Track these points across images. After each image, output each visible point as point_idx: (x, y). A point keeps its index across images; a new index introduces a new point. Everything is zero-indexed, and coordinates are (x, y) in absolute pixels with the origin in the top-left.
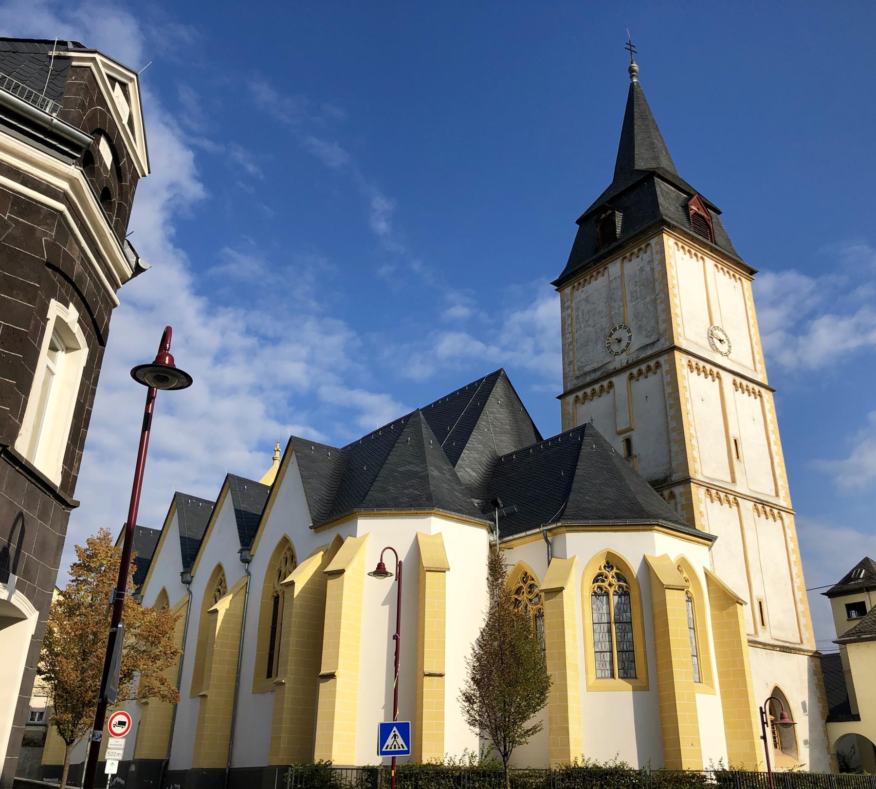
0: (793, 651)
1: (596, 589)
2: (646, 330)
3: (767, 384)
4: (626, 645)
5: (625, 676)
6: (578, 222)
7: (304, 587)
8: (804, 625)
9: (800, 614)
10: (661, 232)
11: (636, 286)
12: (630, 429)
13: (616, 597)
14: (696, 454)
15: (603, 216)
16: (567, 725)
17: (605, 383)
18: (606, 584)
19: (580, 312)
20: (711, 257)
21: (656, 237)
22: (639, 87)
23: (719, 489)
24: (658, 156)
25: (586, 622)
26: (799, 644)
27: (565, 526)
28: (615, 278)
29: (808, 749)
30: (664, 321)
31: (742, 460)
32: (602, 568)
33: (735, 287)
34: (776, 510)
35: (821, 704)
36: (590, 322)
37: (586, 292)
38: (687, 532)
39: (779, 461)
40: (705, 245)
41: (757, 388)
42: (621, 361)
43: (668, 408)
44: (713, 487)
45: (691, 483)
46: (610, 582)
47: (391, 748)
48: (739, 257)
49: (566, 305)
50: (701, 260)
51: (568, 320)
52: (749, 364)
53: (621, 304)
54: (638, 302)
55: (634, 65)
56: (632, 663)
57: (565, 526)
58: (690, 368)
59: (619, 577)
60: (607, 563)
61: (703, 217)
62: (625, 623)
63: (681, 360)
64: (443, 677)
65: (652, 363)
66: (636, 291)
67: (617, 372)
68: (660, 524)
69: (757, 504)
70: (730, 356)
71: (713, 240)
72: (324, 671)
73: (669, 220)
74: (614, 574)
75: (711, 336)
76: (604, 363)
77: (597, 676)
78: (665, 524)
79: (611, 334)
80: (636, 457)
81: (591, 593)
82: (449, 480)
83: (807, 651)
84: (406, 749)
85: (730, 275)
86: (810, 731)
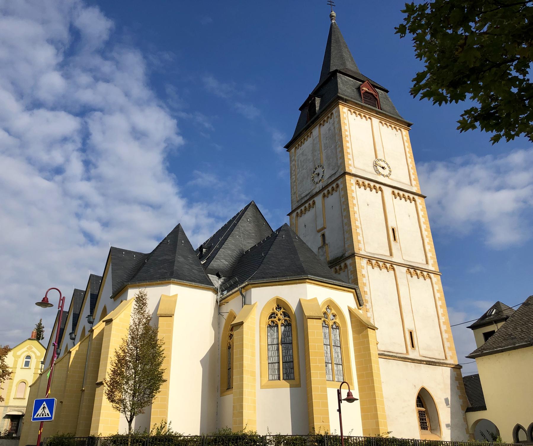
1: (270, 323)
3: (420, 193)
4: (289, 358)
5: (288, 378)
6: (300, 109)
7: (100, 332)
9: (445, 340)
10: (337, 105)
11: (327, 140)
12: (324, 228)
13: (283, 327)
14: (360, 238)
15: (310, 101)
17: (311, 202)
18: (276, 319)
20: (376, 117)
23: (378, 260)
24: (345, 62)
25: (262, 344)
26: (443, 360)
27: (251, 284)
28: (316, 137)
29: (450, 431)
30: (340, 158)
31: (398, 241)
32: (275, 309)
36: (304, 167)
37: (303, 149)
38: (333, 283)
40: (372, 110)
41: (411, 196)
42: (319, 187)
43: (343, 210)
44: (373, 258)
45: (356, 257)
47: (40, 416)
48: (399, 116)
49: (292, 159)
52: (408, 182)
53: (319, 153)
54: (328, 150)
55: (333, 12)
56: (292, 370)
57: (251, 284)
58: (359, 186)
59: (285, 314)
60: (278, 306)
61: (372, 94)
62: (288, 343)
63: (350, 180)
65: (334, 185)
66: (327, 143)
67: (317, 194)
70: (391, 177)
72: (99, 381)
73: (343, 96)
74: (282, 313)
75: (375, 165)
77: (269, 379)
78: (313, 278)
79: (314, 171)
82: (192, 264)
83: (450, 364)
84: (50, 416)
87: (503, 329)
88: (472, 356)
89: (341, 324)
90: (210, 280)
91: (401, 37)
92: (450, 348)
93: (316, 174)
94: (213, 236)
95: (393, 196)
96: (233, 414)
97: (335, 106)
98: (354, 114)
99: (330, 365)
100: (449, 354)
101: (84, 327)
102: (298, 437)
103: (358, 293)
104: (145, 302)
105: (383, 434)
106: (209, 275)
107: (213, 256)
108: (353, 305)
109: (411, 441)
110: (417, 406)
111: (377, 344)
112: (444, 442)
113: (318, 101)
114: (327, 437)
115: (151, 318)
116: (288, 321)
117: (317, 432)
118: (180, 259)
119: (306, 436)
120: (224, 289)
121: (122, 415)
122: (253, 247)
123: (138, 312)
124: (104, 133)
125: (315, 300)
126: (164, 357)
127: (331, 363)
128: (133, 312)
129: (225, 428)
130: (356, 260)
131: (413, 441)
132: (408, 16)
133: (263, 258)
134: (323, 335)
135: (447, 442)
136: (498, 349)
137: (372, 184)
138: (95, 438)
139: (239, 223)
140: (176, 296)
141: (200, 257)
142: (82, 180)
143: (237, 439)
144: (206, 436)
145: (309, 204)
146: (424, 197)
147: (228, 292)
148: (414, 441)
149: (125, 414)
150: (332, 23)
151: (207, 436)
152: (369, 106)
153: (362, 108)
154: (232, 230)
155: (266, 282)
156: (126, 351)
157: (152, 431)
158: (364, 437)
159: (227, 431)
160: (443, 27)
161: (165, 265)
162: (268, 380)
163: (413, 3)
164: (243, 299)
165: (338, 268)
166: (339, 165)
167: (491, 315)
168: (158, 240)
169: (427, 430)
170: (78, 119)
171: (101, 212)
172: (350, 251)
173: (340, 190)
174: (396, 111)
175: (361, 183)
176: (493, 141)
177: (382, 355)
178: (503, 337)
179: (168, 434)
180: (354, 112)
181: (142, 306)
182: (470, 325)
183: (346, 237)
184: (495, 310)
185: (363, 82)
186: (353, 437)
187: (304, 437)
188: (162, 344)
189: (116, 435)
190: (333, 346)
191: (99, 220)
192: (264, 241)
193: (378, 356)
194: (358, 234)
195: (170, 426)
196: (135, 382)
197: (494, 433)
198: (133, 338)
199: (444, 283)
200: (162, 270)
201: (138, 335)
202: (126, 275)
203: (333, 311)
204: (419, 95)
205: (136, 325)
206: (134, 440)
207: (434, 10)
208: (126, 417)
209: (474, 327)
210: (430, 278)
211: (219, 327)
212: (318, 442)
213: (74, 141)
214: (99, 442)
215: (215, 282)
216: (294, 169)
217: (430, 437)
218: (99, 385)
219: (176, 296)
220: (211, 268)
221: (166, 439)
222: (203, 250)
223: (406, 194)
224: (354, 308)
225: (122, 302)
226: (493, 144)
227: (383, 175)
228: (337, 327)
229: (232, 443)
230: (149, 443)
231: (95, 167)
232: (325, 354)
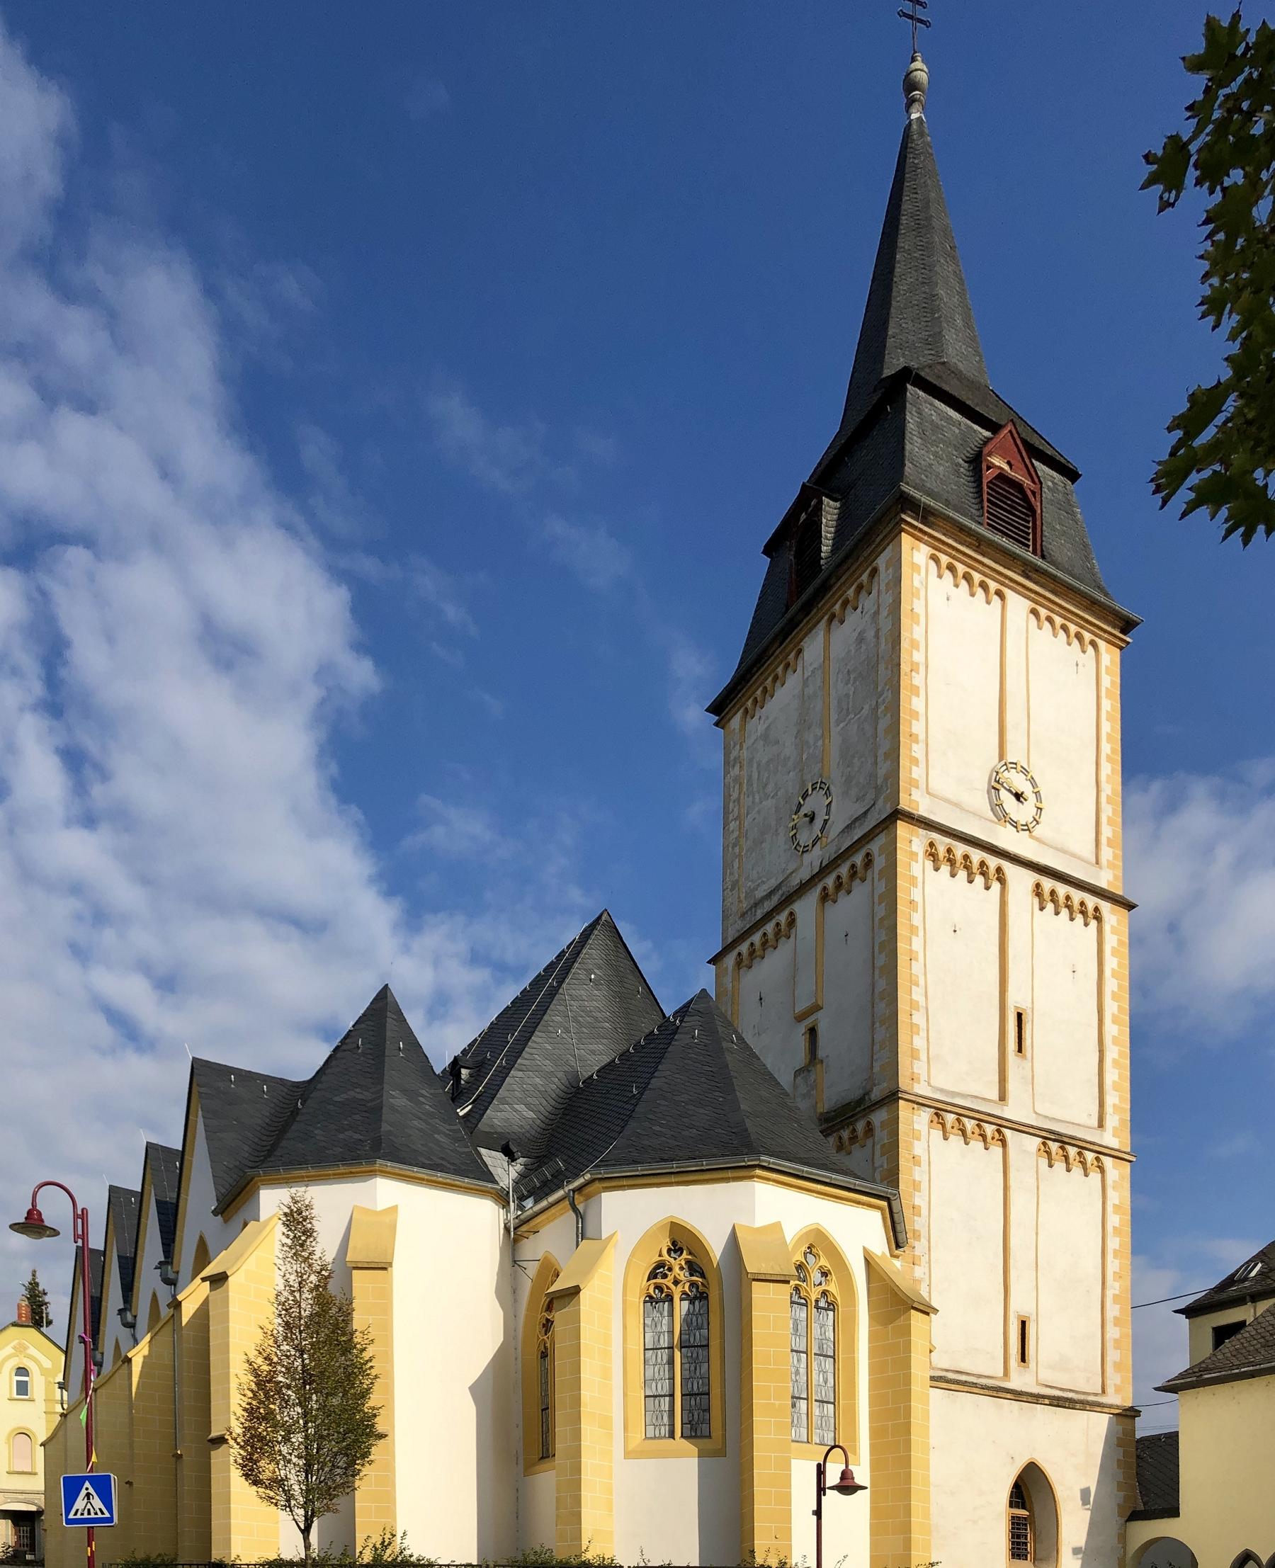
0: (1078, 1406)
1: (651, 1291)
3: (1119, 892)
5: (693, 1434)
6: (767, 551)
12: (816, 1008)
13: (686, 1304)
14: (919, 1042)
15: (803, 516)
16: (579, 1509)
17: (782, 918)
18: (668, 1282)
21: (888, 545)
22: (922, 134)
23: (962, 1113)
26: (1096, 1395)
27: (600, 1179)
30: (887, 756)
31: (1029, 1055)
33: (1077, 665)
34: (1008, 1130)
36: (770, 788)
38: (828, 1180)
41: (1091, 901)
44: (949, 1108)
46: (675, 1276)
47: (82, 1514)
48: (1100, 588)
50: (996, 599)
51: (734, 791)
52: (1087, 850)
53: (819, 733)
57: (600, 1179)
59: (693, 1268)
60: (674, 1243)
61: (1018, 486)
62: (697, 1346)
63: (910, 841)
64: (386, 1438)
65: (858, 859)
67: (804, 887)
68: (765, 1164)
69: (1050, 1143)
70: (1038, 831)
71: (1038, 547)
74: (683, 1263)
75: (995, 786)
76: (788, 872)
77: (647, 1436)
78: (773, 1163)
79: (800, 806)
83: (1110, 1406)
84: (107, 1515)
85: (955, 576)
90: (486, 1166)
91: (1165, 205)
92: (1118, 1366)
93: (806, 815)
95: (1036, 900)
99: (803, 1404)
100: (1113, 1379)
101: (154, 1295)
104: (309, 1226)
106: (483, 1151)
108: (878, 1243)
110: (1011, 1506)
111: (931, 1351)
113: (830, 511)
115: (331, 1272)
116: (701, 1288)
118: (395, 1099)
120: (525, 1193)
121: (284, 1516)
122: (606, 1066)
123: (294, 1254)
125: (776, 1227)
126: (376, 1377)
129: (538, 1549)
130: (901, 1113)
136: (1243, 1370)
137: (977, 855)
140: (394, 1209)
141: (453, 1094)
142: (68, 823)
147: (536, 1202)
149: (290, 1513)
154: (544, 1009)
156: (275, 1359)
157: (361, 1553)
159: (543, 1556)
164: (577, 1223)
165: (845, 1134)
167: (1246, 1279)
168: (327, 1039)
169: (1027, 1559)
171: (144, 940)
172: (885, 1085)
175: (942, 851)
177: (939, 1381)
178: (1263, 1337)
179: (400, 1558)
181: (303, 1238)
183: (878, 1037)
184: (1260, 1265)
185: (994, 427)
188: (366, 1342)
189: (275, 1560)
190: (815, 1354)
191: (144, 967)
193: (929, 1382)
194: (914, 1029)
195: (404, 1541)
198: (287, 1325)
200: (349, 1133)
203: (823, 1262)
204: (1184, 495)
205: (294, 1291)
209: (1191, 1312)
210: (1102, 1169)
211: (515, 1301)
216: (735, 795)
218: (217, 1443)
219: (394, 1209)
222: (460, 1073)
223: (1077, 896)
224: (879, 1254)
225: (245, 1225)
227: (1015, 824)
228: (829, 1304)
232: (793, 1375)
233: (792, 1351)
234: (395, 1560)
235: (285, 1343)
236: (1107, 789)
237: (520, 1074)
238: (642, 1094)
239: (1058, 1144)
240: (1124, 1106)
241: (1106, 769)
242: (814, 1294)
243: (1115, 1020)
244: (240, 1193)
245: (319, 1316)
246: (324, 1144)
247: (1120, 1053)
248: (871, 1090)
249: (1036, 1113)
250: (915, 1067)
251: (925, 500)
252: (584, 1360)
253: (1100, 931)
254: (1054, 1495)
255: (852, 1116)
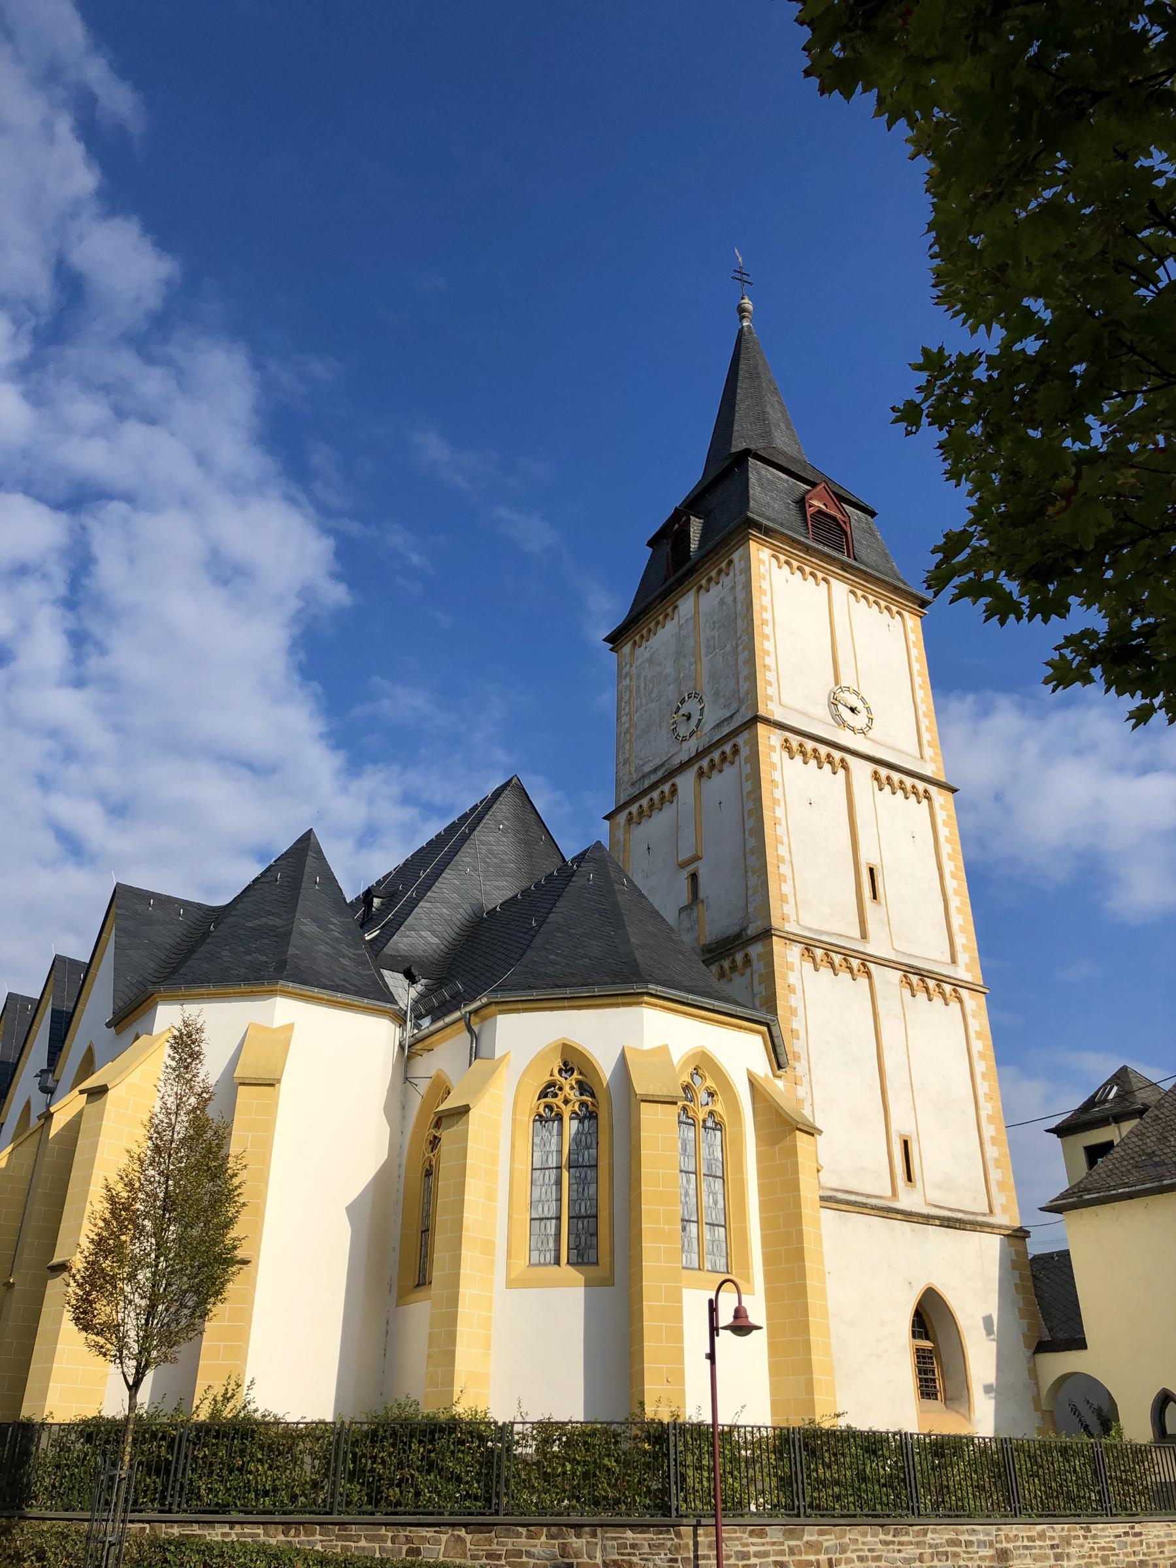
0: (968, 1227)
2: (724, 696)
3: (943, 779)
5: (580, 1260)
6: (650, 544)
8: (998, 1182)
9: (991, 1165)
10: (745, 540)
12: (696, 858)
13: (575, 1123)
14: (786, 889)
15: (677, 526)
17: (666, 788)
18: (558, 1101)
19: (642, 679)
23: (829, 948)
26: (984, 1215)
27: (497, 1003)
29: (993, 1402)
30: (746, 678)
32: (556, 1072)
35: (1025, 1321)
36: (654, 695)
38: (711, 1007)
39: (959, 905)
40: (831, 560)
41: (921, 786)
44: (818, 944)
48: (900, 580)
50: (823, 583)
52: (913, 748)
55: (746, 300)
57: (497, 1003)
59: (583, 1088)
60: (565, 1064)
61: (834, 518)
62: (586, 1166)
65: (727, 748)
67: (683, 767)
68: (654, 992)
69: (910, 976)
70: (871, 734)
73: (760, 520)
74: (574, 1083)
75: (834, 702)
78: (660, 991)
79: (679, 708)
80: (703, 901)
81: (532, 1118)
82: (337, 940)
83: (1000, 1227)
86: (999, 1368)
87: (1133, 1140)
88: (1055, 1208)
89: (728, 1116)
90: (387, 986)
91: (908, 433)
92: (1001, 1185)
93: (683, 715)
94: (404, 864)
95: (875, 783)
96: (429, 1356)
97: (737, 543)
98: (785, 567)
99: (693, 1228)
100: (999, 1199)
101: (28, 1103)
102: (599, 1426)
103: (775, 1034)
104: (197, 1048)
105: (824, 1418)
106: (385, 972)
107: (399, 919)
108: (761, 1065)
109: (894, 1437)
110: (914, 1336)
111: (818, 1171)
112: (978, 1438)
113: (696, 527)
114: (675, 1428)
115: (213, 1094)
116: (590, 1107)
117: (650, 1412)
118: (305, 926)
119: (621, 1423)
120: (423, 1012)
121: (114, 1370)
122: (510, 899)
123: (177, 1076)
124: (131, 560)
125: (664, 1050)
126: (244, 1204)
127: (697, 1222)
128: (162, 1078)
129: (403, 1400)
130: (775, 947)
131: (897, 1437)
132: (928, 381)
133: (532, 933)
134: (680, 1146)
135: (984, 1439)
136: (1120, 1191)
137: (823, 750)
138: (33, 1425)
139: (475, 833)
140: (290, 1027)
141: (363, 919)
142: (60, 684)
143: (432, 1432)
144: (347, 1421)
145: (662, 792)
146: (954, 791)
147: (433, 1022)
148: (901, 1436)
149: (120, 1365)
150: (743, 327)
151: (351, 1423)
152: (826, 549)
153: (806, 553)
154: (455, 851)
155: (537, 1000)
156: (137, 1185)
157: (197, 1407)
158: (774, 1429)
159: (407, 1409)
160: (1017, 419)
161: (263, 941)
162: (527, 1263)
163: (941, 349)
164: (472, 1043)
165: (726, 964)
166: (741, 696)
167: (1105, 1101)
168: (261, 860)
169: (937, 1399)
170: (63, 518)
171: (106, 775)
173: (743, 763)
174: (893, 566)
175: (795, 746)
176: (1134, 720)
177: (829, 1201)
178: (1133, 1158)
179: (242, 1415)
180: (787, 563)
181: (189, 1060)
182: (1053, 1126)
184: (1115, 1088)
185: (813, 485)
186: (745, 1427)
187: (613, 1427)
188: (239, 1167)
189: (94, 1417)
190: (704, 1175)
191: (101, 797)
192: (537, 885)
193: (818, 1202)
194: (781, 878)
195: (250, 1392)
196: (154, 1274)
197: (1103, 1407)
198: (157, 1149)
199: (994, 1006)
200: (257, 955)
201: (172, 1142)
202: (152, 965)
203: (710, 1083)
204: (949, 591)
205: (170, 1114)
206: (145, 1432)
207: (995, 375)
208: (123, 1373)
209: (1061, 1131)
210: (960, 1000)
211: (404, 1117)
212: (652, 1439)
213: (45, 577)
214: (44, 1436)
215: (401, 991)
216: (626, 698)
217: (946, 1424)
218: (59, 1270)
219: (290, 1027)
220: (393, 953)
221: (237, 1432)
222: (372, 901)
223: (909, 781)
224: (762, 1075)
225: (137, 1038)
226: (1134, 727)
227: (853, 729)
228: (716, 1124)
229: (420, 1442)
230: (188, 1440)
231: (103, 651)
232: (683, 1198)
233: (681, 1171)
234: (236, 1417)
235: (151, 1168)
236: (922, 708)
237: (428, 905)
238: (540, 927)
239: (917, 977)
240: (971, 945)
241: (920, 694)
242: (702, 1114)
243: (954, 876)
244: (139, 1006)
245: (193, 1139)
246: (228, 964)
247: (962, 902)
248: (747, 927)
249: (894, 949)
250: (784, 908)
251: (765, 522)
252: (470, 1181)
253: (931, 807)
254: (956, 1324)
255: (732, 948)
